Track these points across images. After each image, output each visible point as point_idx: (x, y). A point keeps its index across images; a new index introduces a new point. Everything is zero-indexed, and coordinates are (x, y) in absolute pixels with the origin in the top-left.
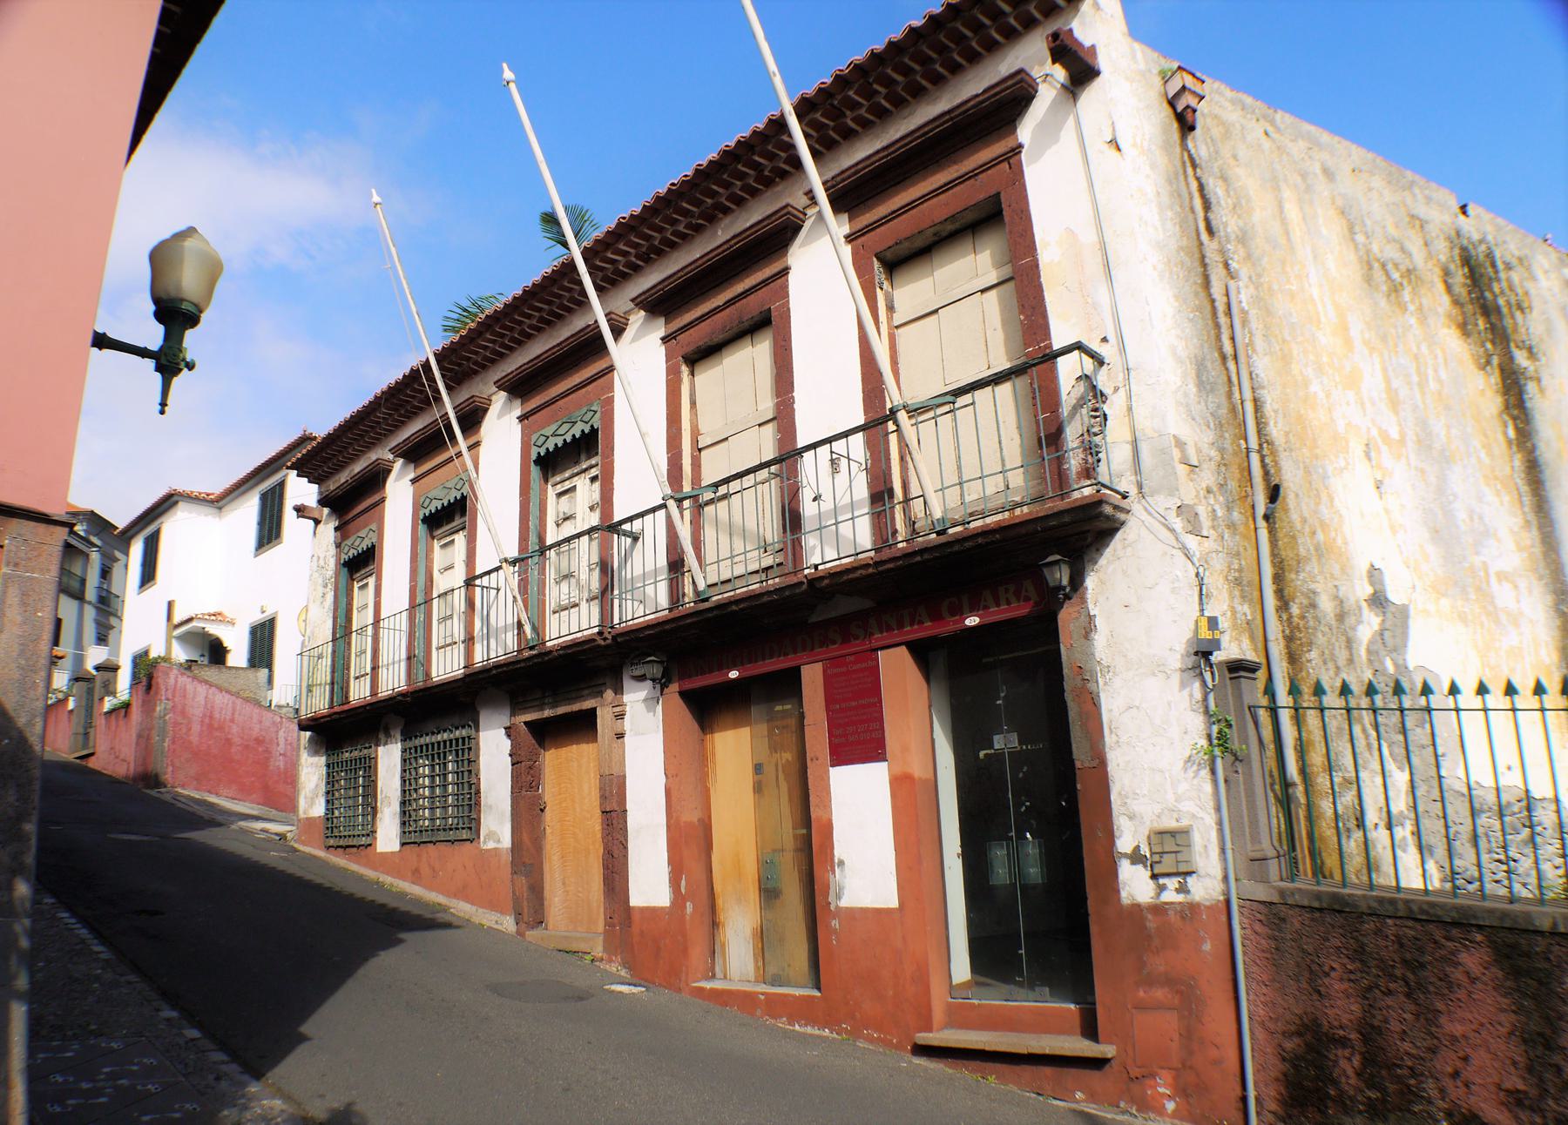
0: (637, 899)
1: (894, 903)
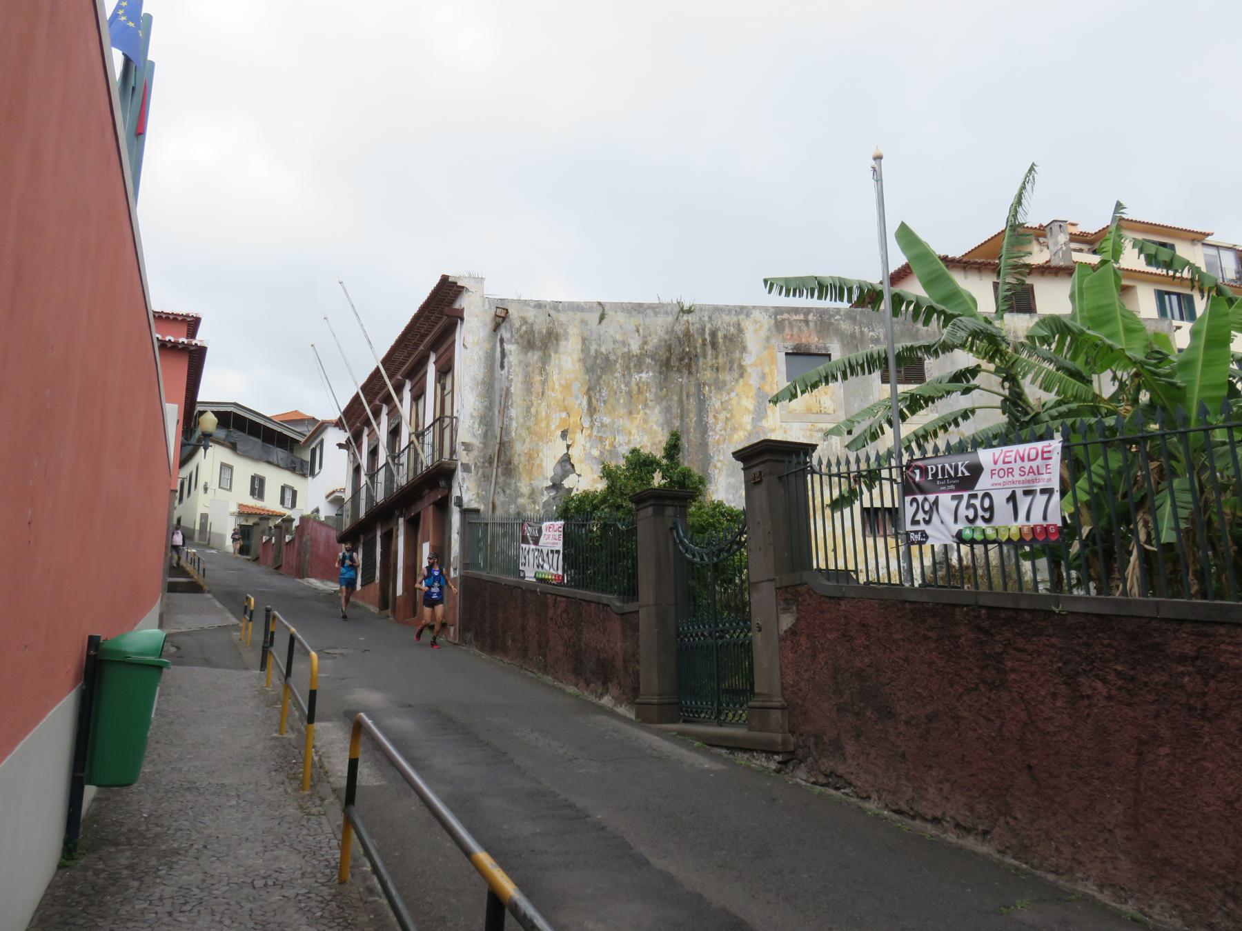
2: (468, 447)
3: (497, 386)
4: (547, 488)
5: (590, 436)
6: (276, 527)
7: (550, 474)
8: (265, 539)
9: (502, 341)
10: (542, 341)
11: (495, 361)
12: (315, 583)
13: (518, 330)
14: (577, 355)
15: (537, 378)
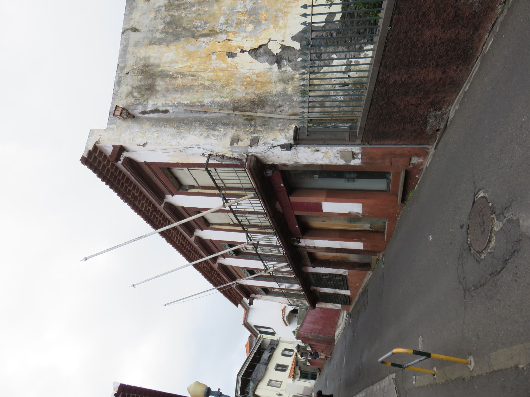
0: (362, 248)
2: (235, 140)
3: (182, 116)
4: (280, 67)
5: (234, 33)
6: (302, 356)
7: (267, 65)
8: (308, 364)
9: (144, 113)
10: (148, 79)
11: (162, 118)
12: (338, 332)
13: (136, 99)
14: (163, 48)
15: (179, 81)
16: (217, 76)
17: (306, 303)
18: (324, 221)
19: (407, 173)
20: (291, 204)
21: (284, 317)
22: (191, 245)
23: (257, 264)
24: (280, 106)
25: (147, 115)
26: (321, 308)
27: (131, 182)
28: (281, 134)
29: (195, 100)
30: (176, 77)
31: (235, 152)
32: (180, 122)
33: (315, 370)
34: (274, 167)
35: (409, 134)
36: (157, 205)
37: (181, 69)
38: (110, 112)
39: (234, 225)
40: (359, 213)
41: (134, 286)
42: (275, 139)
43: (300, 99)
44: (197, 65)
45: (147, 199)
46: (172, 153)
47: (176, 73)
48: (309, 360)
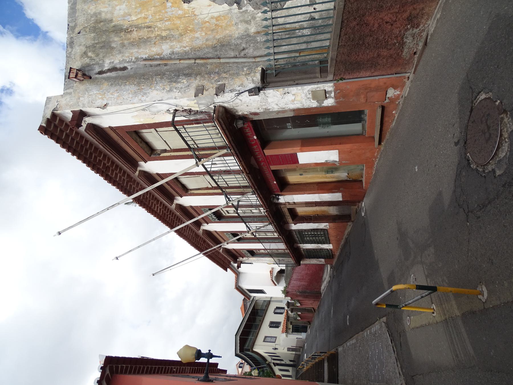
0: (341, 199)
1: (337, 151)
4: (240, 8)
6: (292, 312)
8: (299, 318)
9: (100, 73)
11: (121, 75)
12: (324, 286)
15: (135, 35)
16: (174, 24)
17: (291, 261)
18: (301, 175)
19: (383, 108)
20: (267, 157)
21: (272, 277)
22: (173, 213)
23: (240, 227)
24: (244, 49)
25: (104, 75)
26: (306, 265)
27: (101, 152)
28: (247, 79)
29: (153, 53)
30: (131, 31)
31: (201, 104)
32: (140, 78)
33: (305, 323)
34: (244, 118)
35: (385, 60)
36: (132, 175)
37: (135, 22)
38: (65, 76)
39: (213, 188)
40: (336, 161)
41: (117, 258)
42: (242, 85)
43: (264, 39)
44: (152, 16)
45: (121, 169)
46: (136, 113)
47: (130, 26)
48: (299, 315)
